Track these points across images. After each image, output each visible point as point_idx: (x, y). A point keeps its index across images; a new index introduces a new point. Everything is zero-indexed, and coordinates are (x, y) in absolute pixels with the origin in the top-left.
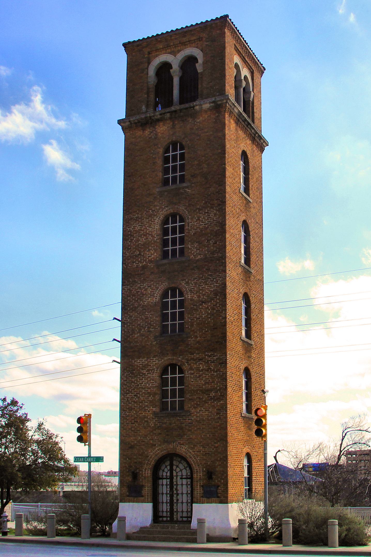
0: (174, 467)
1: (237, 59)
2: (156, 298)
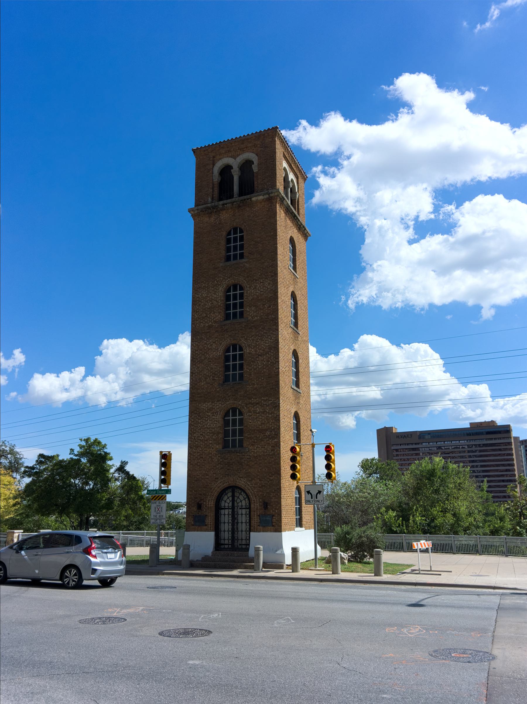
0: (236, 498)
1: (285, 165)
2: (220, 352)
